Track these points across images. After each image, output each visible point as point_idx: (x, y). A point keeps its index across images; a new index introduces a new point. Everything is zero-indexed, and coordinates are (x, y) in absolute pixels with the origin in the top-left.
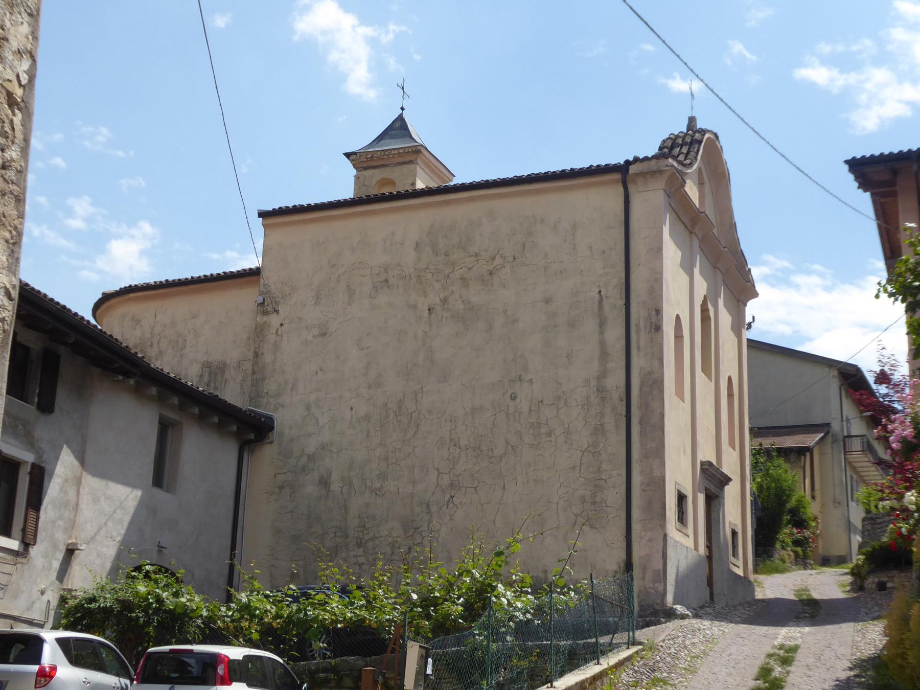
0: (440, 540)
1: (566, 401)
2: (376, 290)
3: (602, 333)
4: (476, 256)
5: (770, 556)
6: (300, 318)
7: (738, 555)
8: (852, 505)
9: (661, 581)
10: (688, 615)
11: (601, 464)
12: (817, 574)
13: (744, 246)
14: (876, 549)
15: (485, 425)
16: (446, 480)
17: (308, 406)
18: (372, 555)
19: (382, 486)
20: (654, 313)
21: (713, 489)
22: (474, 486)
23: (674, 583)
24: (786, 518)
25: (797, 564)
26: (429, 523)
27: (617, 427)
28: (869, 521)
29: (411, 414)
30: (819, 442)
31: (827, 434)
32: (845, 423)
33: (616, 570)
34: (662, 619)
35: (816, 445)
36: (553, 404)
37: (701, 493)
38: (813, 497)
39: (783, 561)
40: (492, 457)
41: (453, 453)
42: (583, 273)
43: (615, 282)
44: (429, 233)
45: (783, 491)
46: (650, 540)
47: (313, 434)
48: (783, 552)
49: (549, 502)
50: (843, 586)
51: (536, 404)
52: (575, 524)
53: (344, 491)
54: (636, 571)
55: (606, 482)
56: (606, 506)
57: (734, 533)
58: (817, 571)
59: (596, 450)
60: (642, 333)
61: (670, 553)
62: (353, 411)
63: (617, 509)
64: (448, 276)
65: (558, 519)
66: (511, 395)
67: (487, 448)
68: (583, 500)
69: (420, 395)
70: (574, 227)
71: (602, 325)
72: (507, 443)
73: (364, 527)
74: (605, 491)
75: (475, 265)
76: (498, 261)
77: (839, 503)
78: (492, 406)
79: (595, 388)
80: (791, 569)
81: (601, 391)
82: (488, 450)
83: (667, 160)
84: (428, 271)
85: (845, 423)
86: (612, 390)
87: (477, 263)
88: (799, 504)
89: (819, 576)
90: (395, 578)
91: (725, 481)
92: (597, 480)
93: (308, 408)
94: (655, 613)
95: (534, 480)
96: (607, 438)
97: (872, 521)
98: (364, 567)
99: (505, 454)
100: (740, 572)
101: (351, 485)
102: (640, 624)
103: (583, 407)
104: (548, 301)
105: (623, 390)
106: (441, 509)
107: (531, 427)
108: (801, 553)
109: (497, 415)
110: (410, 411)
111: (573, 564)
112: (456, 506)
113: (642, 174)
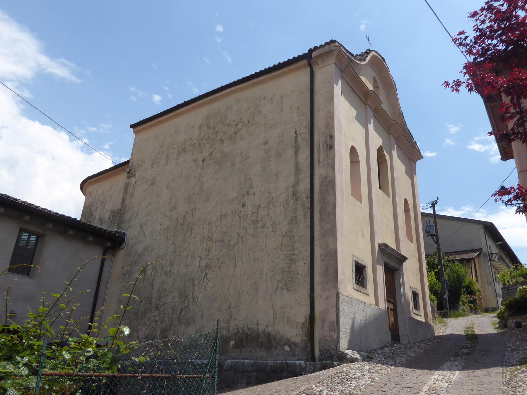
0: (198, 303)
1: (274, 203)
2: (179, 155)
3: (296, 156)
4: (229, 125)
5: (457, 308)
6: (144, 177)
7: (419, 308)
8: (497, 284)
9: (335, 330)
10: (356, 359)
11: (294, 243)
12: (481, 317)
13: (410, 127)
14: (512, 301)
15: (227, 225)
16: (204, 264)
17: (142, 226)
18: (162, 315)
19: (171, 270)
20: (329, 138)
21: (393, 264)
22: (218, 266)
23: (349, 332)
24: (463, 290)
25: (471, 312)
26: (193, 293)
27: (305, 217)
28: (506, 289)
29: (189, 223)
30: (476, 256)
31: (481, 253)
32: (489, 248)
33: (303, 322)
34: (335, 363)
35: (476, 257)
36: (266, 207)
37: (380, 265)
38: (477, 281)
39: (464, 311)
40: (230, 246)
41: (209, 245)
42: (286, 122)
43: (305, 124)
44: (207, 118)
45: (460, 277)
46: (327, 298)
47: (142, 241)
48: (463, 307)
49: (261, 273)
50: (494, 324)
51: (256, 208)
52: (277, 289)
53: (152, 275)
54: (318, 322)
55: (298, 256)
56: (298, 274)
57: (415, 295)
58: (482, 315)
59: (292, 235)
60: (321, 152)
61: (343, 307)
62: (162, 226)
63: (304, 276)
64: (214, 139)
65: (267, 286)
66: (242, 204)
67: (227, 240)
68: (283, 271)
69: (194, 211)
70: (282, 97)
71: (297, 152)
72: (239, 235)
73: (160, 296)
74: (297, 263)
75: (228, 130)
76: (240, 125)
77: (490, 284)
78: (232, 213)
79: (292, 192)
80: (468, 315)
81: (295, 193)
82: (228, 241)
83: (335, 43)
84: (204, 139)
85: (489, 248)
86: (302, 192)
87: (229, 129)
88: (469, 284)
89: (482, 318)
90: (173, 330)
91: (402, 259)
92: (292, 255)
93: (141, 227)
94: (331, 357)
95: (253, 259)
96: (299, 225)
97: (506, 288)
98: (158, 323)
99: (237, 243)
100: (422, 319)
101: (156, 270)
102: (319, 366)
103: (284, 206)
104: (265, 143)
105: (308, 191)
106: (200, 282)
107: (252, 223)
108: (473, 307)
109: (234, 218)
110: (189, 222)
111: (275, 318)
112: (208, 280)
113: (320, 56)
